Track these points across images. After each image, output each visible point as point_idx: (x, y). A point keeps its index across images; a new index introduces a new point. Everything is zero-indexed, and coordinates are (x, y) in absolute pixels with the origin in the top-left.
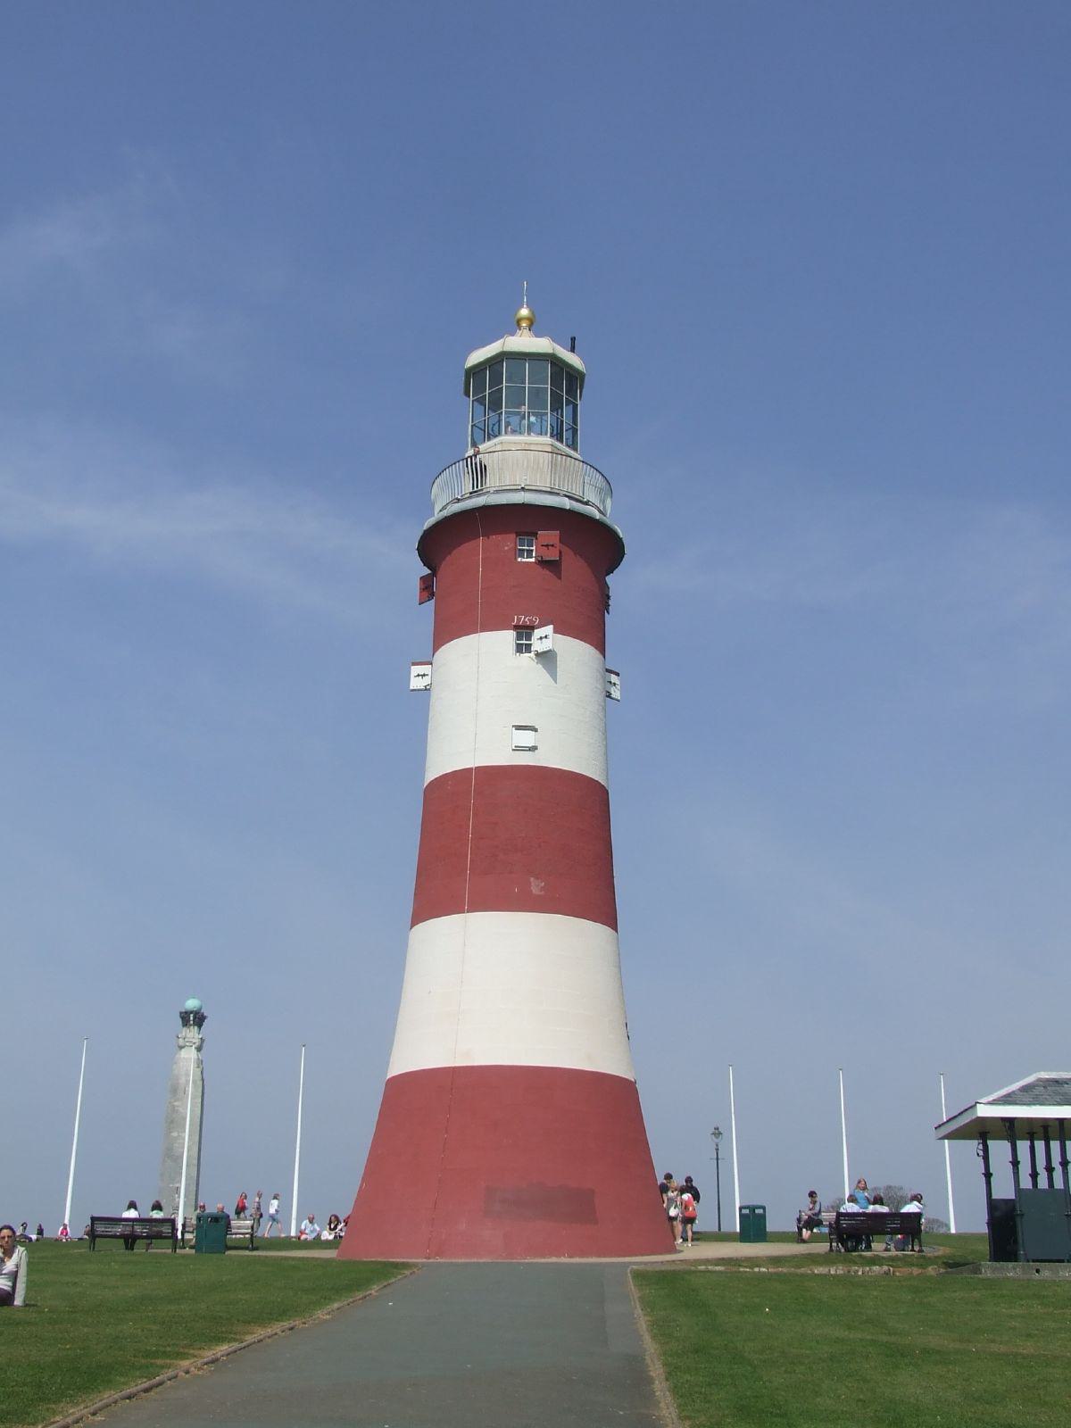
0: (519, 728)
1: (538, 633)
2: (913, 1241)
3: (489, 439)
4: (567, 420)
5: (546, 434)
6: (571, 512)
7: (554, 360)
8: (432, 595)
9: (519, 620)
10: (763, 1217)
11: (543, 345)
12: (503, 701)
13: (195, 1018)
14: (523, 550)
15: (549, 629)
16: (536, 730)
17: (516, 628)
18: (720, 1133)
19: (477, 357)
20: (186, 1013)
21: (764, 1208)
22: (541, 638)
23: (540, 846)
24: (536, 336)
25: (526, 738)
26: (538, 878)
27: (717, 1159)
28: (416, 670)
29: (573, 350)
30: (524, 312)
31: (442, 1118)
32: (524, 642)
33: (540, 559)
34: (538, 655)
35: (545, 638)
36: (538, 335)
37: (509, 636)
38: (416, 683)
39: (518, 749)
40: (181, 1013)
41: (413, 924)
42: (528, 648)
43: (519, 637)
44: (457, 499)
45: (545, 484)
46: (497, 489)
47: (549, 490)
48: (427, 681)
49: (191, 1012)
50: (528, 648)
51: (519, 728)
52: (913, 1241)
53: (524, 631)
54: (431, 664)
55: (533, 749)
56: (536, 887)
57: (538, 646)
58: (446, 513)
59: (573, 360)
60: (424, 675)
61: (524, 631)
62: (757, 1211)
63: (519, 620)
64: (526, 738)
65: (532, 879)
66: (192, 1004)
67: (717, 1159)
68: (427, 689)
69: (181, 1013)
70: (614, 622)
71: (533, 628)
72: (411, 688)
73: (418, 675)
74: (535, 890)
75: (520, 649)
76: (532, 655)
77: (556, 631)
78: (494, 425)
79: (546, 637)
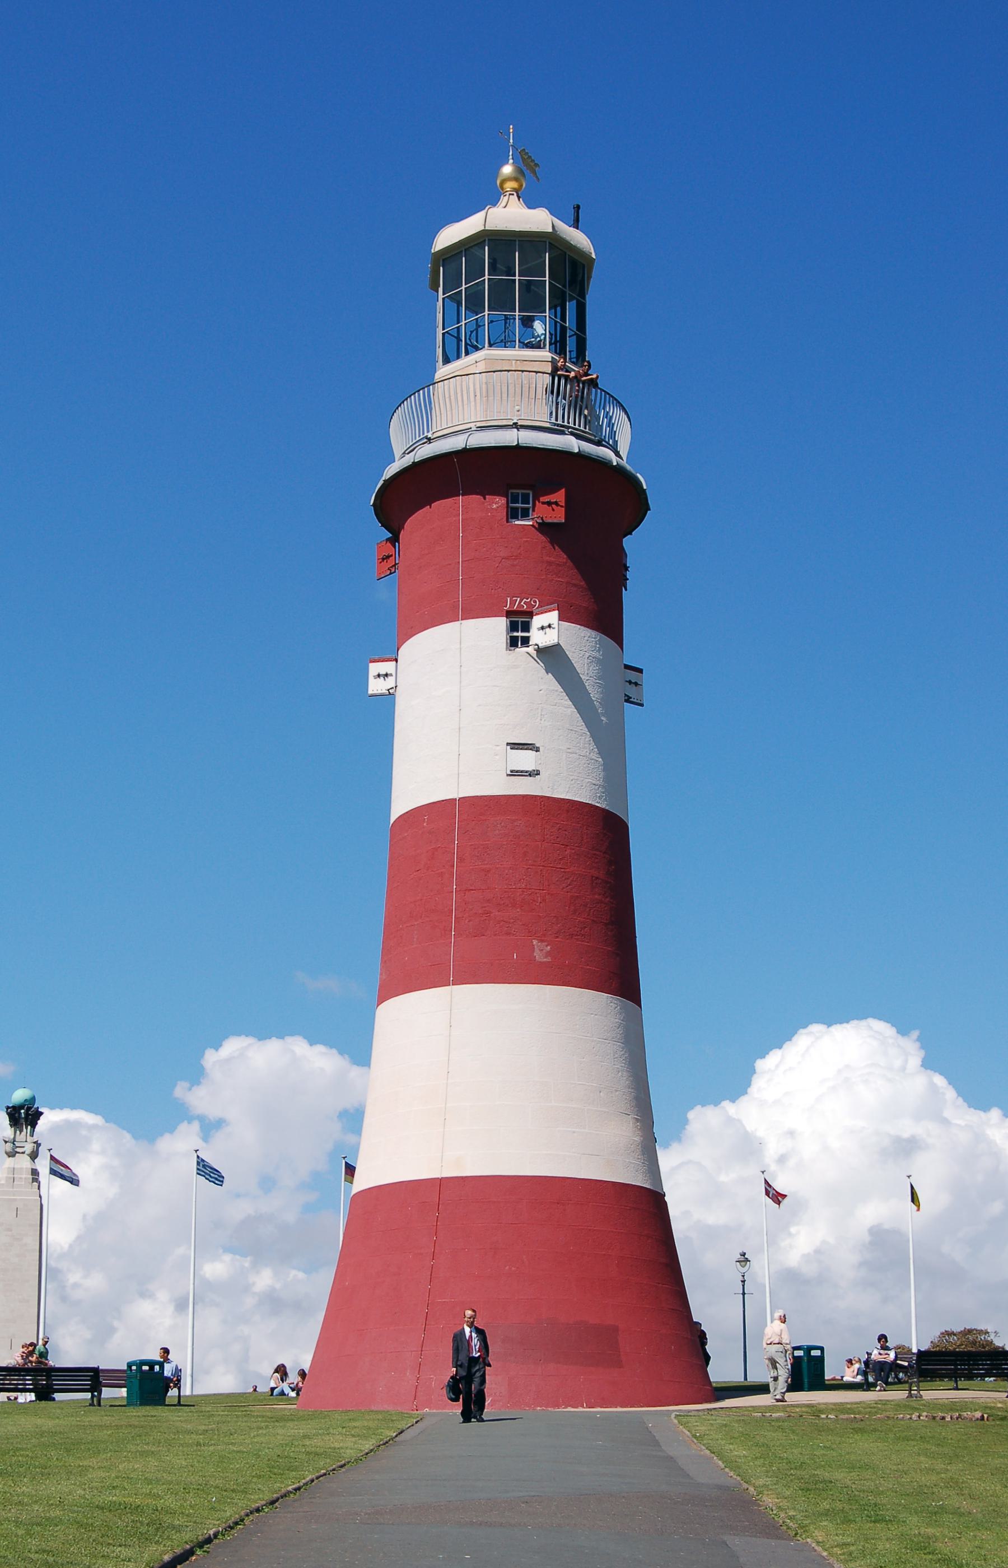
0: (515, 746)
1: (537, 621)
2: (575, 585)
3: (467, 353)
4: (570, 322)
5: (544, 347)
6: (581, 457)
7: (551, 241)
8: (393, 569)
9: (513, 603)
10: (821, 1360)
11: (538, 220)
12: (470, 709)
13: (27, 1114)
14: (517, 508)
15: (553, 617)
16: (537, 750)
17: (509, 614)
18: (747, 1260)
19: (450, 236)
20: (14, 1107)
21: (822, 1349)
22: (542, 628)
23: (544, 900)
24: (529, 208)
25: (525, 760)
26: (542, 941)
27: (744, 1294)
28: (375, 668)
29: (576, 225)
30: (507, 170)
31: (409, 1238)
32: (520, 634)
33: (540, 521)
34: (541, 651)
35: (547, 628)
36: (531, 205)
37: (501, 623)
38: (376, 686)
39: (514, 773)
40: (8, 1108)
41: (380, 1001)
42: (526, 641)
43: (513, 627)
44: (426, 437)
45: (542, 416)
46: (479, 424)
47: (548, 425)
48: (390, 682)
49: (21, 1107)
50: (526, 641)
51: (515, 746)
52: (575, 585)
53: (519, 626)
54: (396, 660)
55: (534, 774)
56: (541, 952)
57: (539, 638)
58: (408, 460)
59: (578, 238)
60: (386, 675)
61: (519, 626)
62: (814, 1353)
63: (513, 603)
64: (525, 760)
65: (535, 942)
66: (19, 1096)
67: (744, 1294)
68: (390, 695)
69: (8, 1108)
70: (632, 600)
71: (531, 614)
72: (370, 692)
73: (379, 676)
74: (539, 956)
75: (513, 643)
76: (530, 649)
77: (561, 618)
78: (472, 332)
79: (549, 626)
